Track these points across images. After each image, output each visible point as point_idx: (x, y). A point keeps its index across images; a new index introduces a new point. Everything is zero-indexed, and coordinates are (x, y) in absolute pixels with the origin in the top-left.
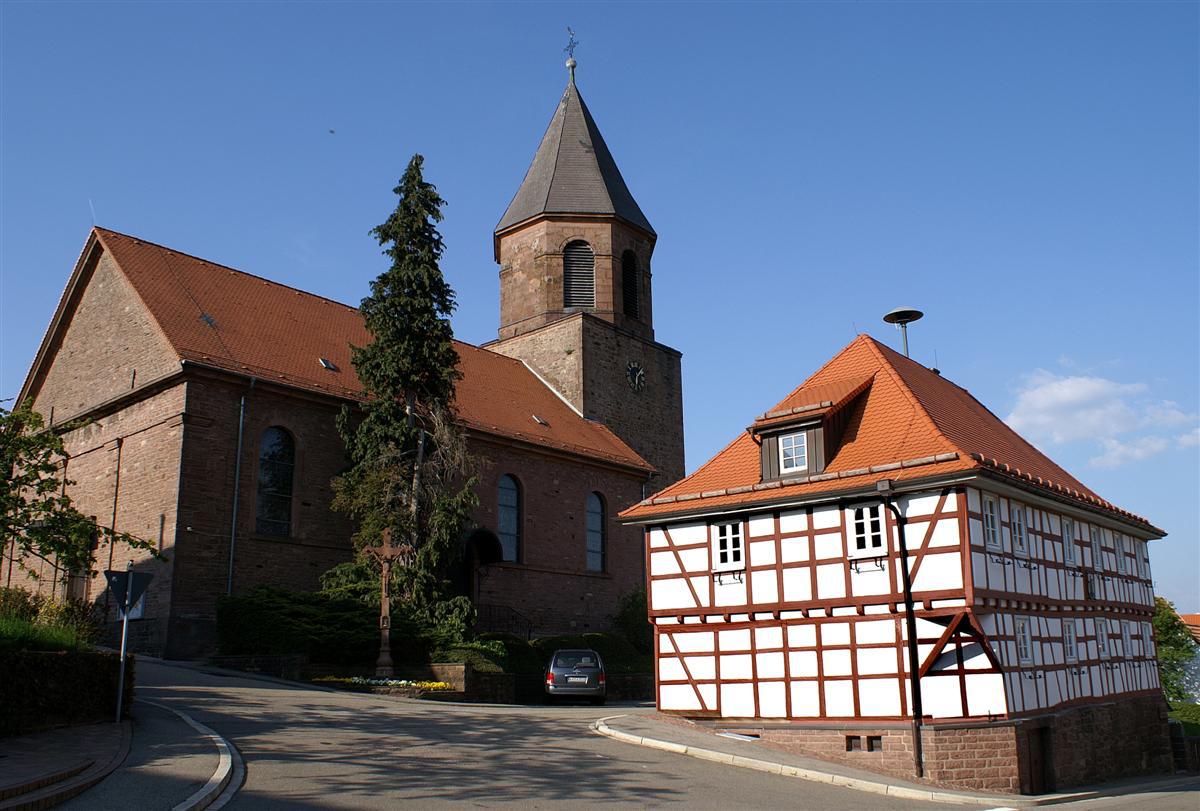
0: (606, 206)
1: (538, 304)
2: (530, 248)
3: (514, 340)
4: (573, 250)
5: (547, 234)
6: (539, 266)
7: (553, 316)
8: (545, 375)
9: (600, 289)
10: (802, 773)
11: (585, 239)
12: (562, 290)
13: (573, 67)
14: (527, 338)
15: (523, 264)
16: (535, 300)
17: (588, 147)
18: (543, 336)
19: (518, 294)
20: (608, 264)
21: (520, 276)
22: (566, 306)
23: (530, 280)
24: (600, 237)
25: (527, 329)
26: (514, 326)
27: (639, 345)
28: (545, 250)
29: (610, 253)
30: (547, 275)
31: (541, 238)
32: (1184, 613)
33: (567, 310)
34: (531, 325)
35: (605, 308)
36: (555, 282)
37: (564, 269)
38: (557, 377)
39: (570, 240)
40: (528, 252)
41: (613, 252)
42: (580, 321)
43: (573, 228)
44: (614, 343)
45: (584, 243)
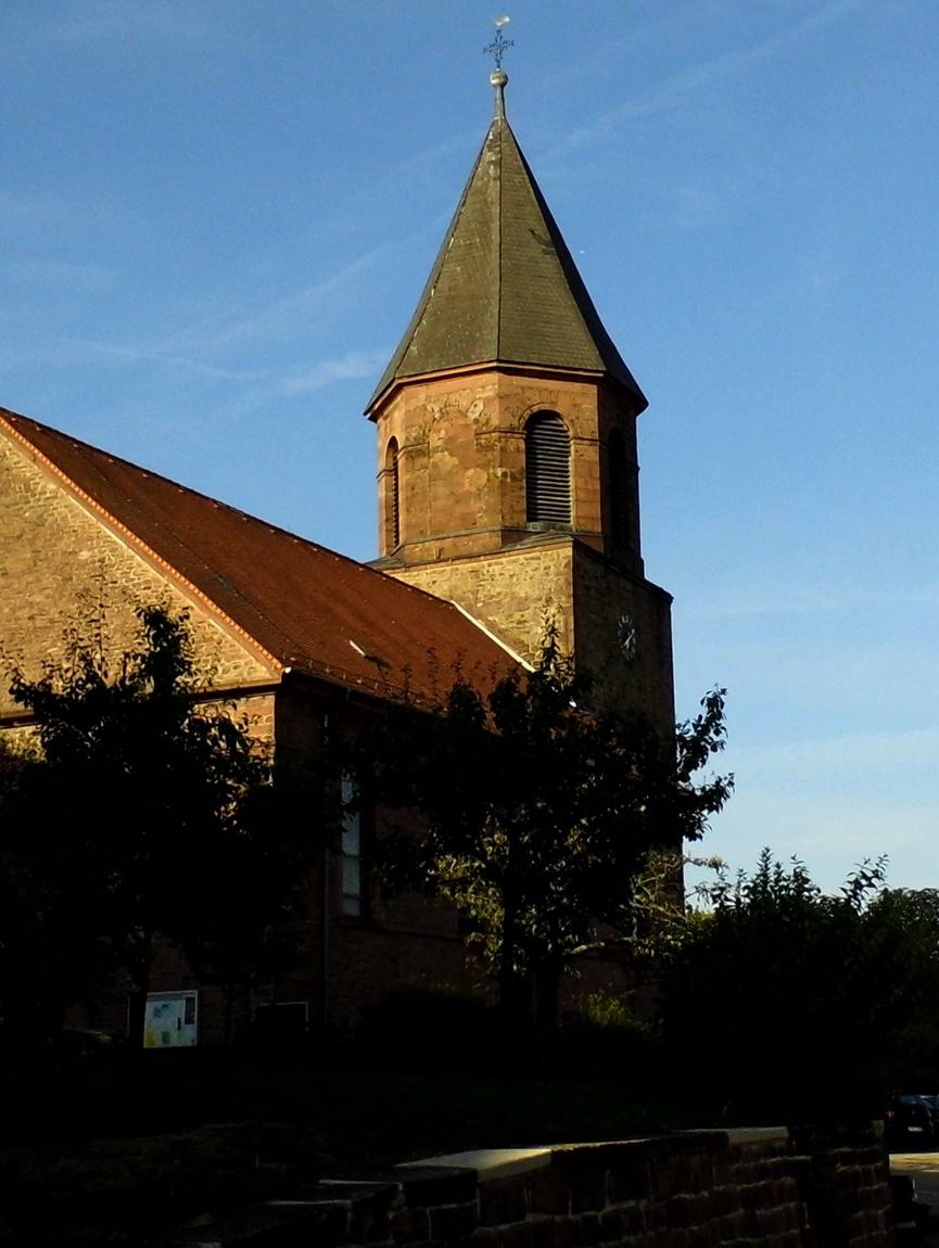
0: (591, 360)
1: (487, 516)
2: (464, 414)
3: (439, 568)
4: (539, 427)
5: (500, 397)
6: (482, 449)
7: (512, 536)
8: (500, 633)
9: (582, 495)
10: (296, 1203)
11: (557, 410)
12: (524, 493)
13: (503, 85)
14: (465, 567)
15: (449, 440)
16: (476, 506)
17: (545, 243)
18: (497, 568)
19: (441, 490)
20: (593, 454)
21: (447, 460)
22: (529, 520)
23: (467, 469)
24: (579, 406)
25: (463, 551)
26: (438, 544)
27: (629, 586)
28: (495, 422)
29: (597, 436)
30: (501, 466)
31: (487, 402)
32: (378, 552)
33: (532, 526)
34: (471, 545)
35: (589, 528)
36: (514, 478)
37: (527, 458)
38: (524, 638)
39: (535, 409)
40: (461, 422)
41: (600, 436)
42: (569, 551)
43: (540, 390)
44: (605, 585)
45: (554, 415)
